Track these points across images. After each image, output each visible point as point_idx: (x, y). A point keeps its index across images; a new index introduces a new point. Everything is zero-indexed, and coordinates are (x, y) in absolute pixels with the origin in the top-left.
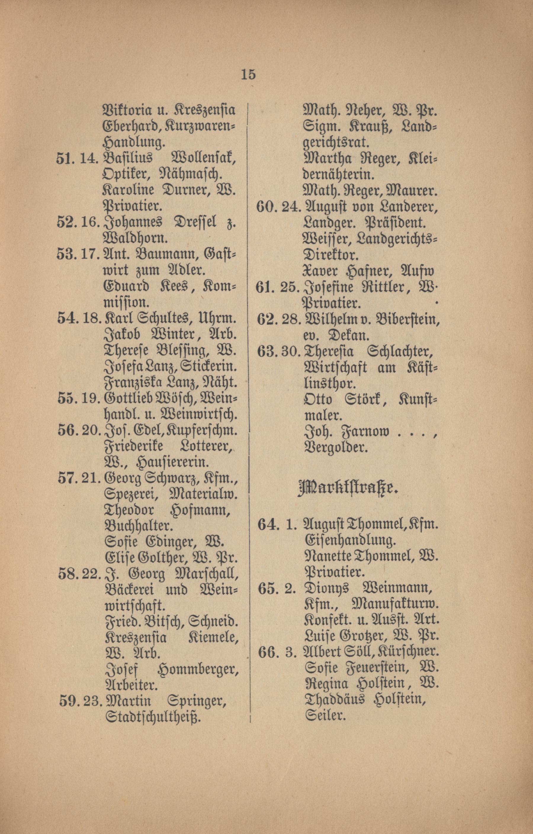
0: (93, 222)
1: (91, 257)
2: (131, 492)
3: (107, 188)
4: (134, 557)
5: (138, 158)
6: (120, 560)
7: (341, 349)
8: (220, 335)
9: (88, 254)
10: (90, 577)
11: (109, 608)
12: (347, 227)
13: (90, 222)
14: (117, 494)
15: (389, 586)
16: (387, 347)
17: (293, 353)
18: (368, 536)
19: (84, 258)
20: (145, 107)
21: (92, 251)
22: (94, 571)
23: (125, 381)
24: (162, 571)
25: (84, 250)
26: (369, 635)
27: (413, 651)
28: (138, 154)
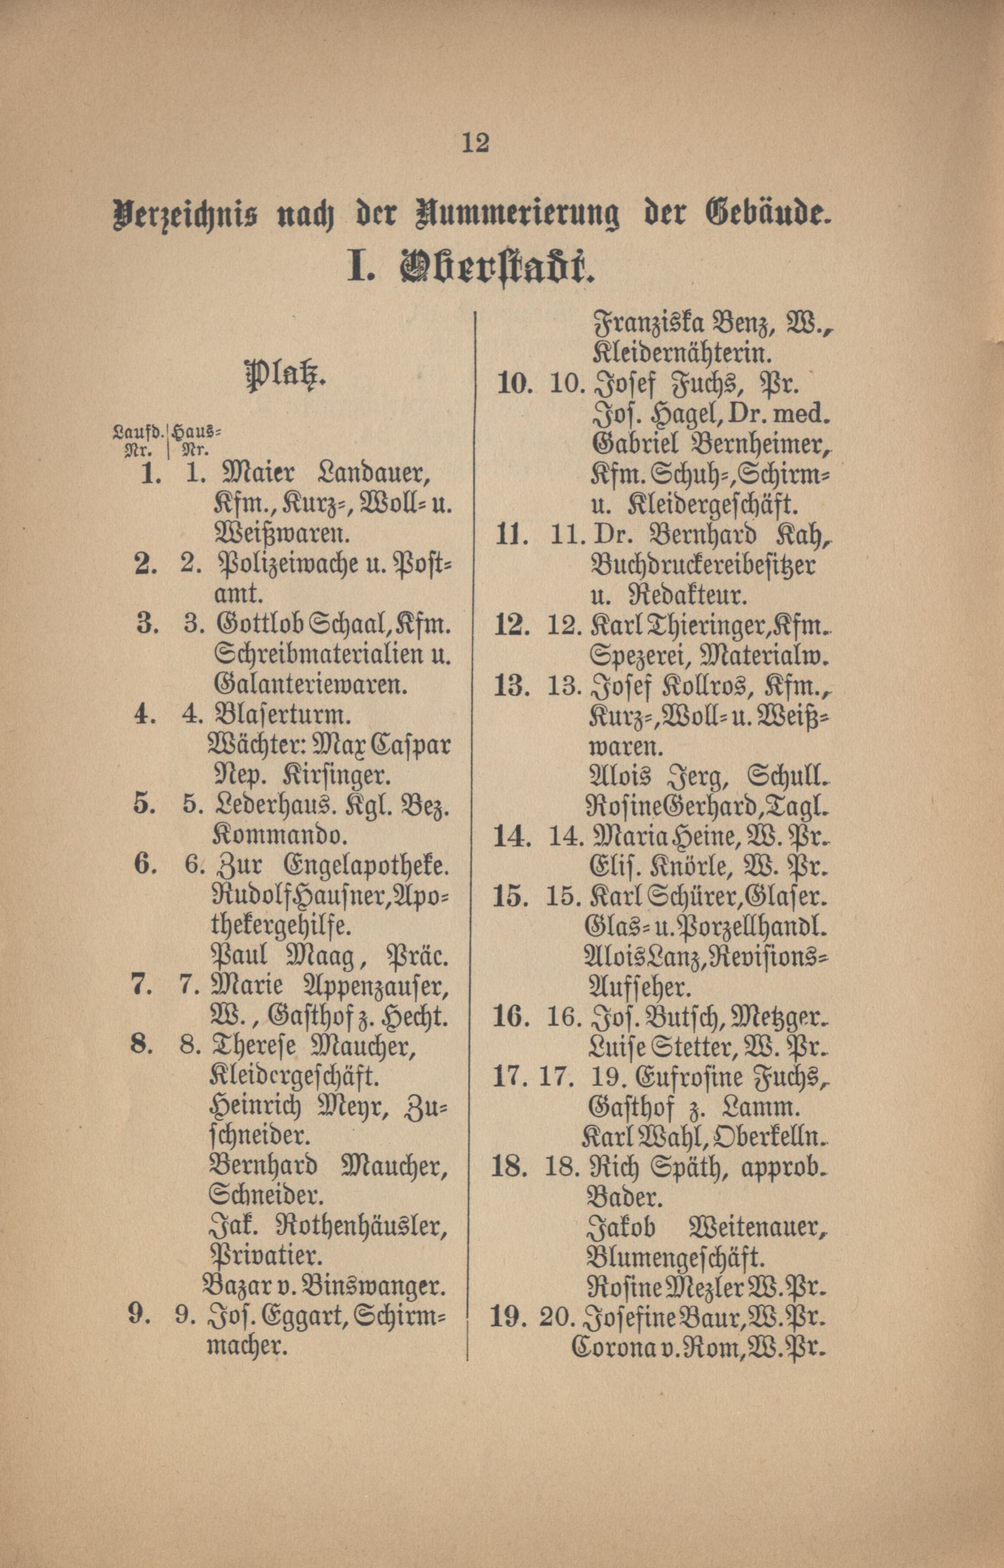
0: (568, 1017)
1: (559, 1083)
2: (641, 652)
3: (600, 621)
4: (644, 1046)
6: (617, 869)
7: (768, 561)
9: (553, 1076)
13: (564, 1017)
14: (613, 656)
19: (545, 1083)
21: (559, 1072)
23: (633, 319)
25: (545, 1069)
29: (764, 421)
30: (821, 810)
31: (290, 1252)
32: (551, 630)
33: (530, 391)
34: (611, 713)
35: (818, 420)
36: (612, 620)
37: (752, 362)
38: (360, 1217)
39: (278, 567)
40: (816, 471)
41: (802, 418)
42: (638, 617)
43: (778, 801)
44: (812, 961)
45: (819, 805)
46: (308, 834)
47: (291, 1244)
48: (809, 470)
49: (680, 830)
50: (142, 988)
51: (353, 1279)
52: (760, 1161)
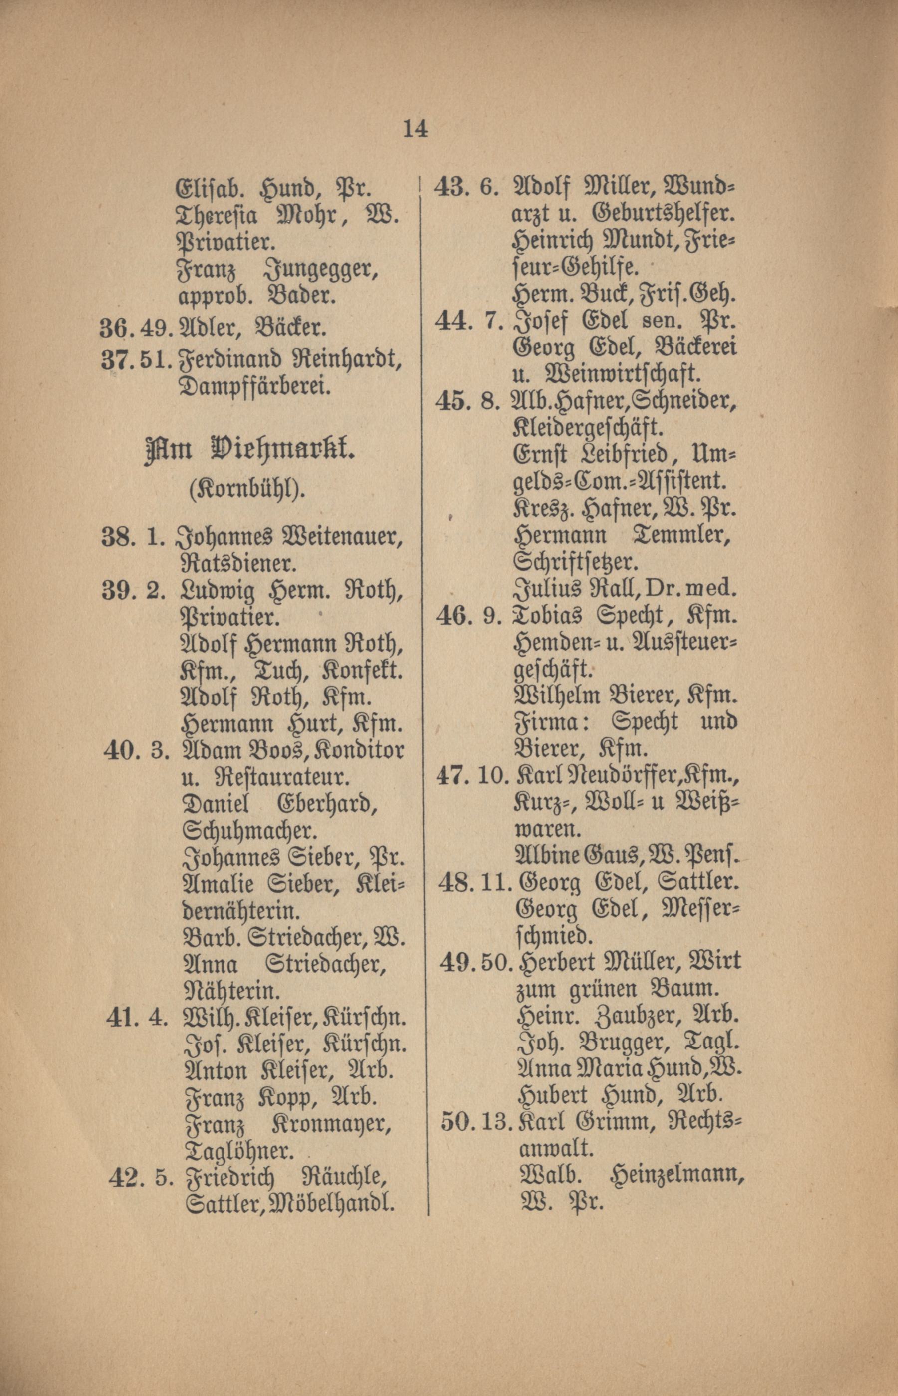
5: (558, 588)
12: (318, 1077)
16: (358, 1170)
24: (576, 878)
27: (383, 1043)
28: (557, 583)
29: (679, 595)
30: (733, 1044)
32: (481, 780)
33: (562, 1049)
35: (727, 593)
36: (536, 770)
40: (724, 451)
41: (712, 592)
42: (558, 768)
43: (695, 1037)
44: (729, 1124)
45: (732, 1040)
48: (721, 691)
52: (580, 409)
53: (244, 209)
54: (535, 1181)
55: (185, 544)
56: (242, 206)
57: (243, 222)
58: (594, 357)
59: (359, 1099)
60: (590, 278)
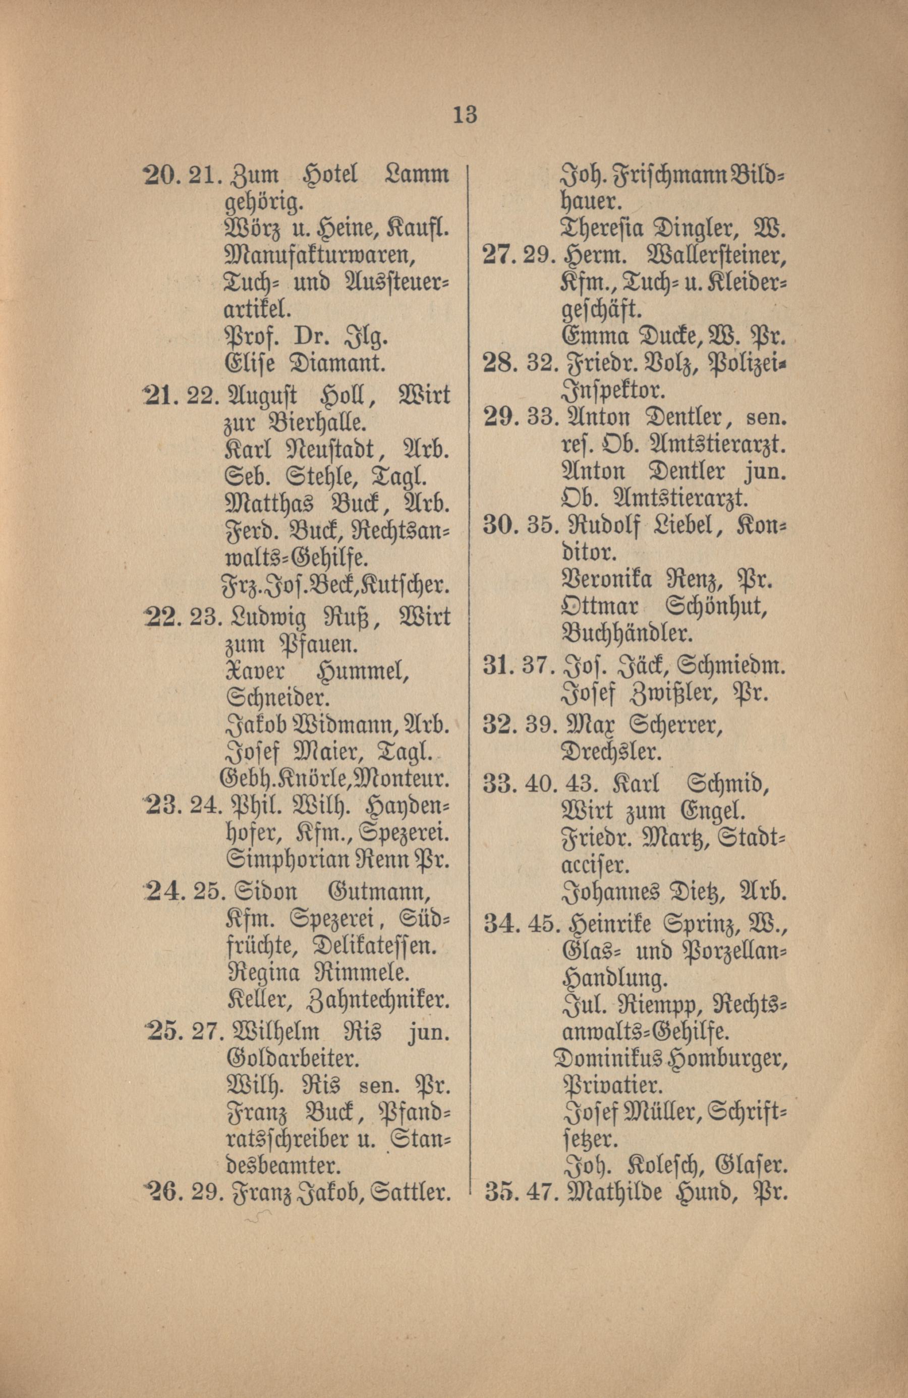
6: (250, 366)
8: (422, 727)
10: (200, 402)
11: (232, 561)
15: (751, 252)
17: (545, 786)
18: (621, 971)
20: (286, 196)
22: (207, 391)
26: (587, 1138)
31: (634, 1082)
34: (380, 581)
37: (604, 932)
38: (732, 598)
39: (732, 955)
46: (599, 978)
47: (635, 1075)
49: (675, 1053)
50: (507, 258)
51: (665, 492)
53: (630, 222)
54: (308, 731)
55: (571, 397)
56: (628, 218)
57: (629, 235)
58: (229, 373)
59: (431, 506)
60: (320, 569)
